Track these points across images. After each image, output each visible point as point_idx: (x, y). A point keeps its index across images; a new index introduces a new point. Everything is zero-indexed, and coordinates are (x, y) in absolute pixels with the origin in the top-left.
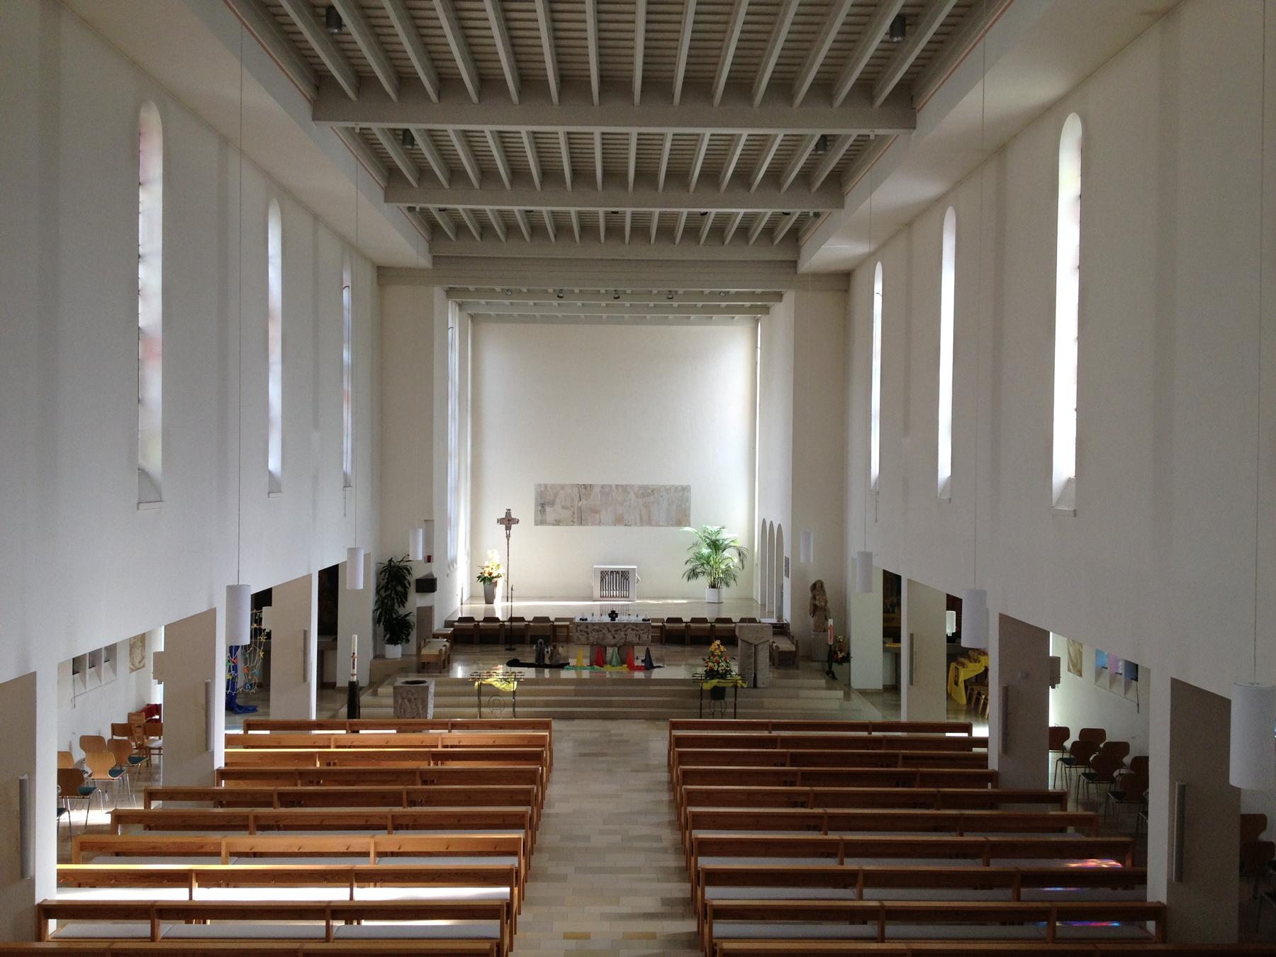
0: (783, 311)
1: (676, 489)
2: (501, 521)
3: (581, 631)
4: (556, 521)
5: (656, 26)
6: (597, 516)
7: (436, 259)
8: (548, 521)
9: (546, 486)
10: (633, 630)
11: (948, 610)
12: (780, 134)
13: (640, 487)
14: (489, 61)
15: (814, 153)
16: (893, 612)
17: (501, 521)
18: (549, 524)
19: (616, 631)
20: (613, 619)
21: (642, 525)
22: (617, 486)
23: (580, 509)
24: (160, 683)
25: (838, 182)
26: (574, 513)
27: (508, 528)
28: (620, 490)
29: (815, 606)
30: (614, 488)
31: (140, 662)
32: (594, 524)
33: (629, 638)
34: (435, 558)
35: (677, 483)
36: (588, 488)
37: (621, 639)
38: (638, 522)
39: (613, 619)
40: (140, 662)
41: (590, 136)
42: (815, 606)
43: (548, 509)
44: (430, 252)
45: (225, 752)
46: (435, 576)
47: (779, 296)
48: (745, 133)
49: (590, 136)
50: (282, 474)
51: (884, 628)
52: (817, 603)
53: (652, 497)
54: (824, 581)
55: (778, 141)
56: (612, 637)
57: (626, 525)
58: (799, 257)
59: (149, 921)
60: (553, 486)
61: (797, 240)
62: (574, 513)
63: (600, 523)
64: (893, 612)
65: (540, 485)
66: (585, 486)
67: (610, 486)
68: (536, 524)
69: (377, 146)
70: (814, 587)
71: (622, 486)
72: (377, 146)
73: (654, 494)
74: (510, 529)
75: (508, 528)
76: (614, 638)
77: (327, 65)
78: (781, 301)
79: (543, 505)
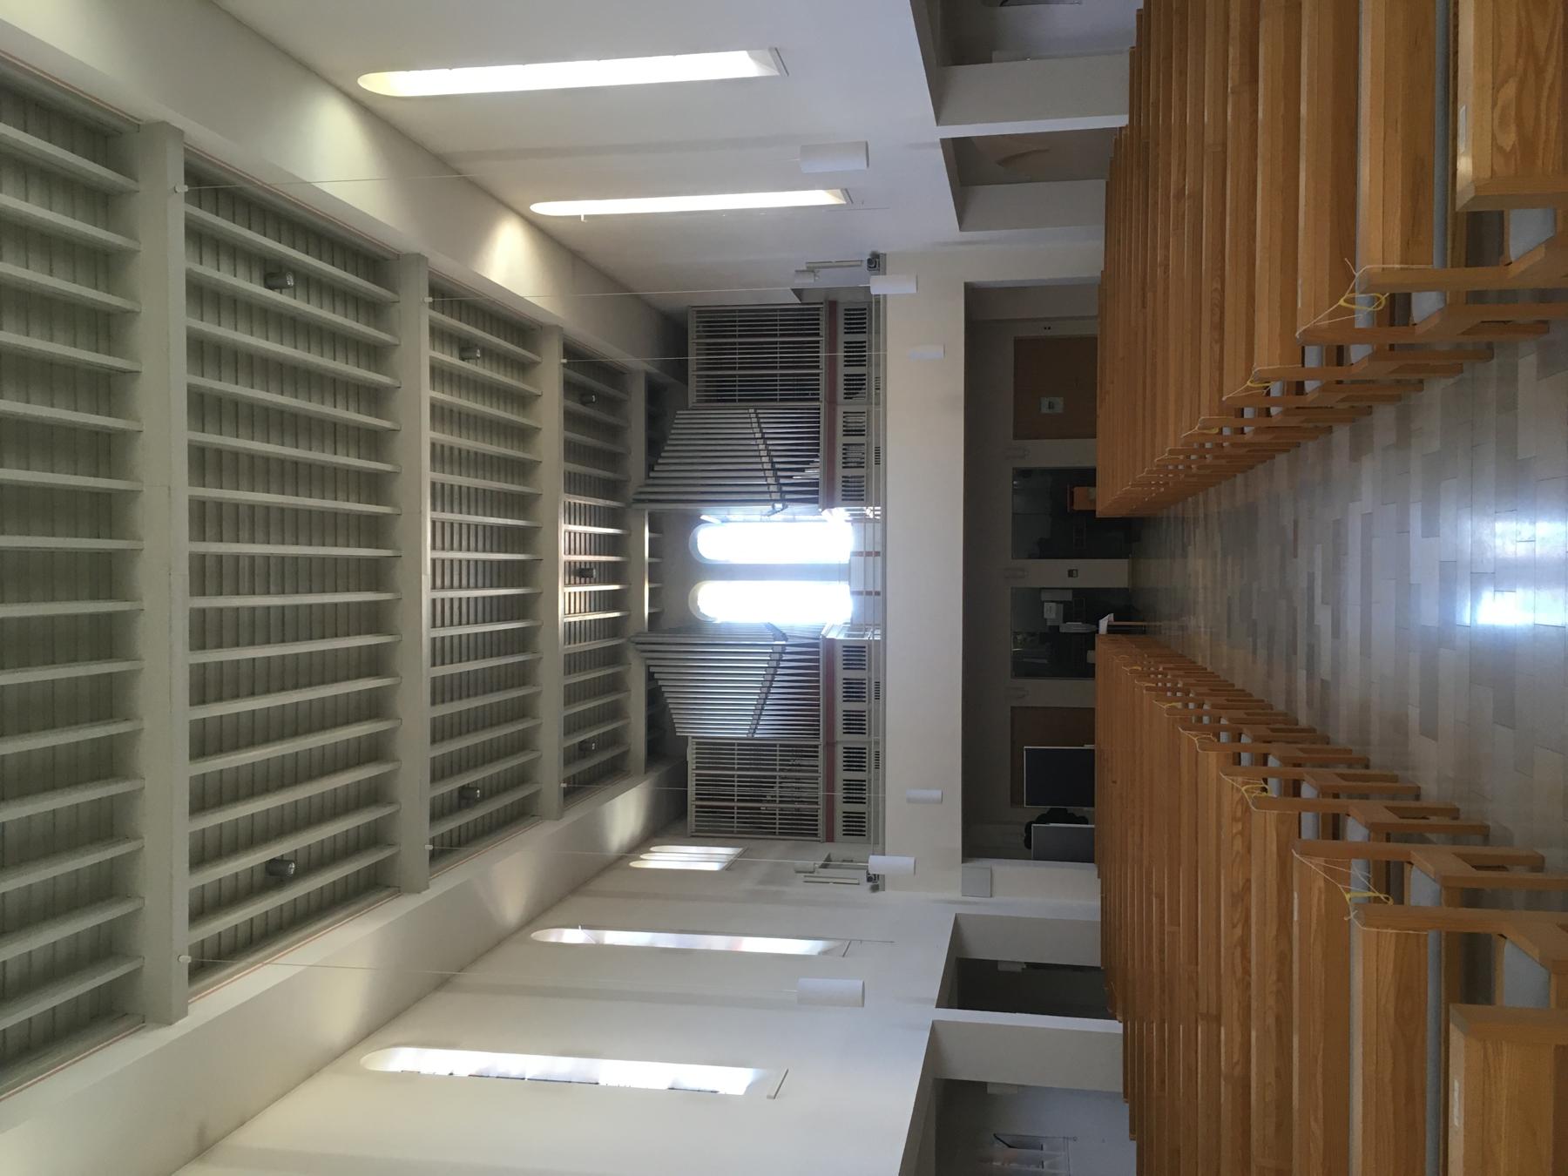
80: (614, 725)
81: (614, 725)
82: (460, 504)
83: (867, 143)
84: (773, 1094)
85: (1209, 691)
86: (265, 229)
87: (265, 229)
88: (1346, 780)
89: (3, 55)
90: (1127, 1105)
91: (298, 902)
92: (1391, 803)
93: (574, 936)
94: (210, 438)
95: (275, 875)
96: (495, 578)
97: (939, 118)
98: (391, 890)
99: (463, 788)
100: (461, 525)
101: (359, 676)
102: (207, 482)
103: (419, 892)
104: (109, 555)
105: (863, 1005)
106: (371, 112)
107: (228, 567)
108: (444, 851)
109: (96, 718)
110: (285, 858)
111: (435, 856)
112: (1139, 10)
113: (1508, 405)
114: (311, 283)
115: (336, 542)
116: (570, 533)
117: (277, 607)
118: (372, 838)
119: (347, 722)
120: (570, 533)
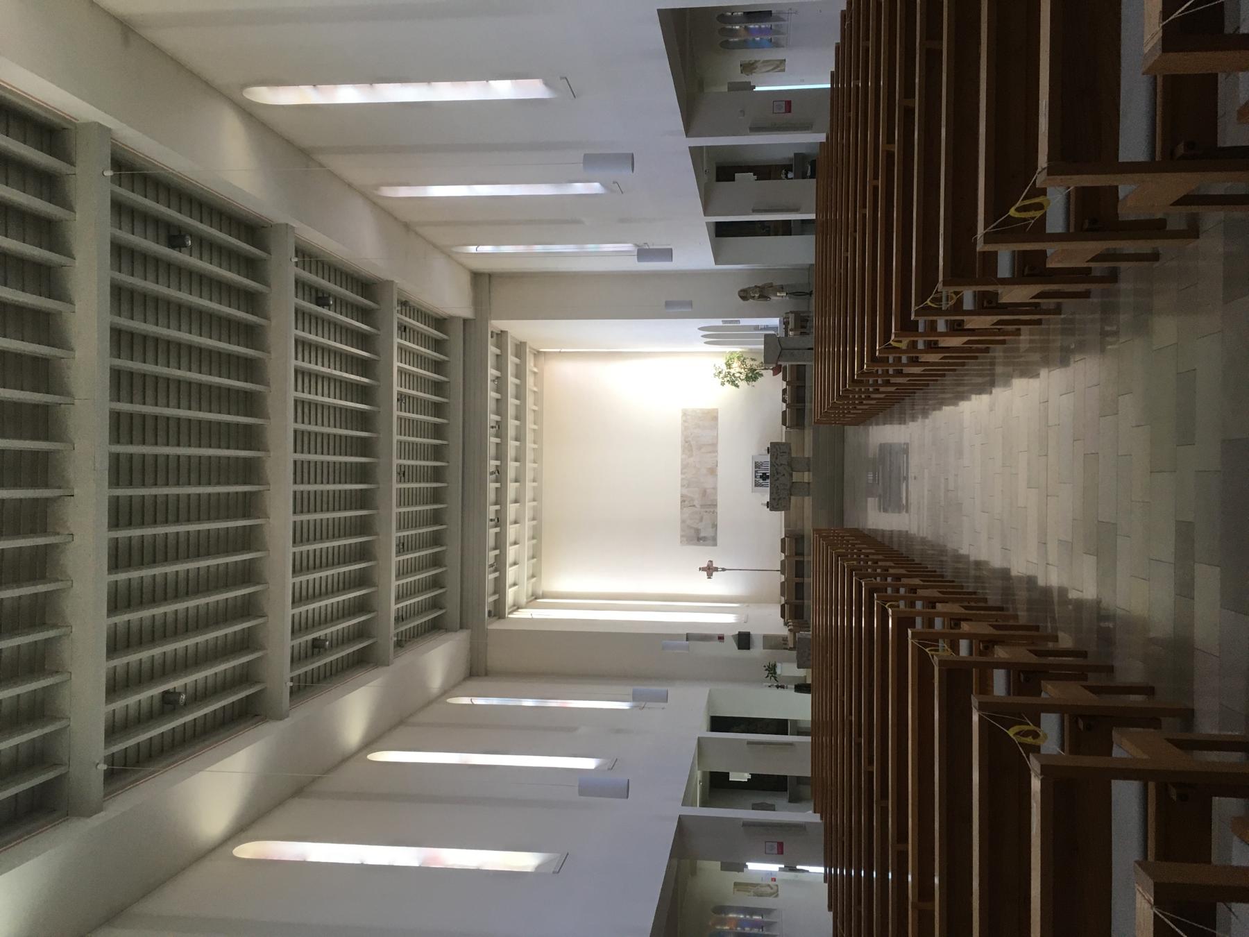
0: (518, 329)
1: (685, 421)
2: (710, 576)
3: (778, 505)
4: (713, 528)
5: (306, 439)
6: (708, 491)
7: (462, 626)
8: (713, 535)
9: (682, 536)
10: (777, 458)
11: (718, 180)
12: (397, 340)
13: (683, 452)
14: (339, 578)
15: (332, 308)
16: (769, 227)
17: (710, 576)
18: (716, 533)
19: (777, 473)
20: (768, 477)
21: (717, 452)
22: (682, 473)
23: (702, 506)
24: (746, 866)
25: (367, 286)
26: (706, 512)
27: (716, 569)
28: (685, 470)
29: (759, 297)
30: (684, 476)
31: (772, 888)
32: (716, 494)
33: (785, 462)
34: (719, 632)
35: (679, 421)
36: (685, 499)
37: (785, 469)
38: (714, 454)
39: (768, 477)
40: (772, 888)
41: (298, 496)
42: (759, 297)
43: (702, 535)
44: (456, 631)
45: (700, 806)
46: (737, 633)
47: (501, 336)
48: (396, 364)
49: (298, 496)
50: (600, 758)
51: (783, 235)
52: (757, 295)
53: (692, 443)
54: (739, 290)
55: (403, 342)
56: (783, 477)
57: (717, 466)
58: (460, 317)
59: (1221, 907)
60: (682, 530)
61: (445, 319)
62: (706, 512)
63: (715, 489)
64: (769, 227)
65: (681, 542)
66: (683, 501)
67: (682, 479)
68: (715, 545)
69: (334, 668)
70: (744, 298)
71: (682, 470)
72: (334, 668)
73: (689, 441)
74: (717, 568)
75: (716, 569)
76: (784, 475)
77: (216, 708)
78: (507, 332)
79: (699, 539)
80: (36, 734)
81: (36, 734)
82: (190, 395)
83: (633, 155)
84: (557, 870)
85: (893, 565)
86: (157, 195)
87: (157, 195)
88: (997, 629)
89: (2, 84)
90: (832, 913)
91: (207, 717)
92: (1030, 648)
93: (465, 701)
94: (126, 364)
95: (169, 704)
96: (343, 477)
97: (689, 130)
98: (258, 718)
99: (166, 693)
100: (335, 436)
101: (345, 536)
102: (212, 409)
103: (281, 720)
104: (47, 454)
105: (627, 797)
106: (253, 117)
107: (137, 465)
108: (303, 688)
109: (361, 534)
110: (177, 691)
111: (293, 692)
112: (842, 11)
113: (905, 421)
114: (207, 246)
115: (200, 443)
116: (401, 442)
117: (224, 493)
118: (244, 677)
119: (328, 566)
120: (401, 442)
